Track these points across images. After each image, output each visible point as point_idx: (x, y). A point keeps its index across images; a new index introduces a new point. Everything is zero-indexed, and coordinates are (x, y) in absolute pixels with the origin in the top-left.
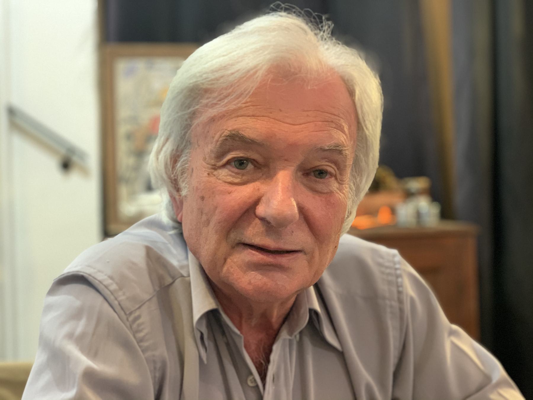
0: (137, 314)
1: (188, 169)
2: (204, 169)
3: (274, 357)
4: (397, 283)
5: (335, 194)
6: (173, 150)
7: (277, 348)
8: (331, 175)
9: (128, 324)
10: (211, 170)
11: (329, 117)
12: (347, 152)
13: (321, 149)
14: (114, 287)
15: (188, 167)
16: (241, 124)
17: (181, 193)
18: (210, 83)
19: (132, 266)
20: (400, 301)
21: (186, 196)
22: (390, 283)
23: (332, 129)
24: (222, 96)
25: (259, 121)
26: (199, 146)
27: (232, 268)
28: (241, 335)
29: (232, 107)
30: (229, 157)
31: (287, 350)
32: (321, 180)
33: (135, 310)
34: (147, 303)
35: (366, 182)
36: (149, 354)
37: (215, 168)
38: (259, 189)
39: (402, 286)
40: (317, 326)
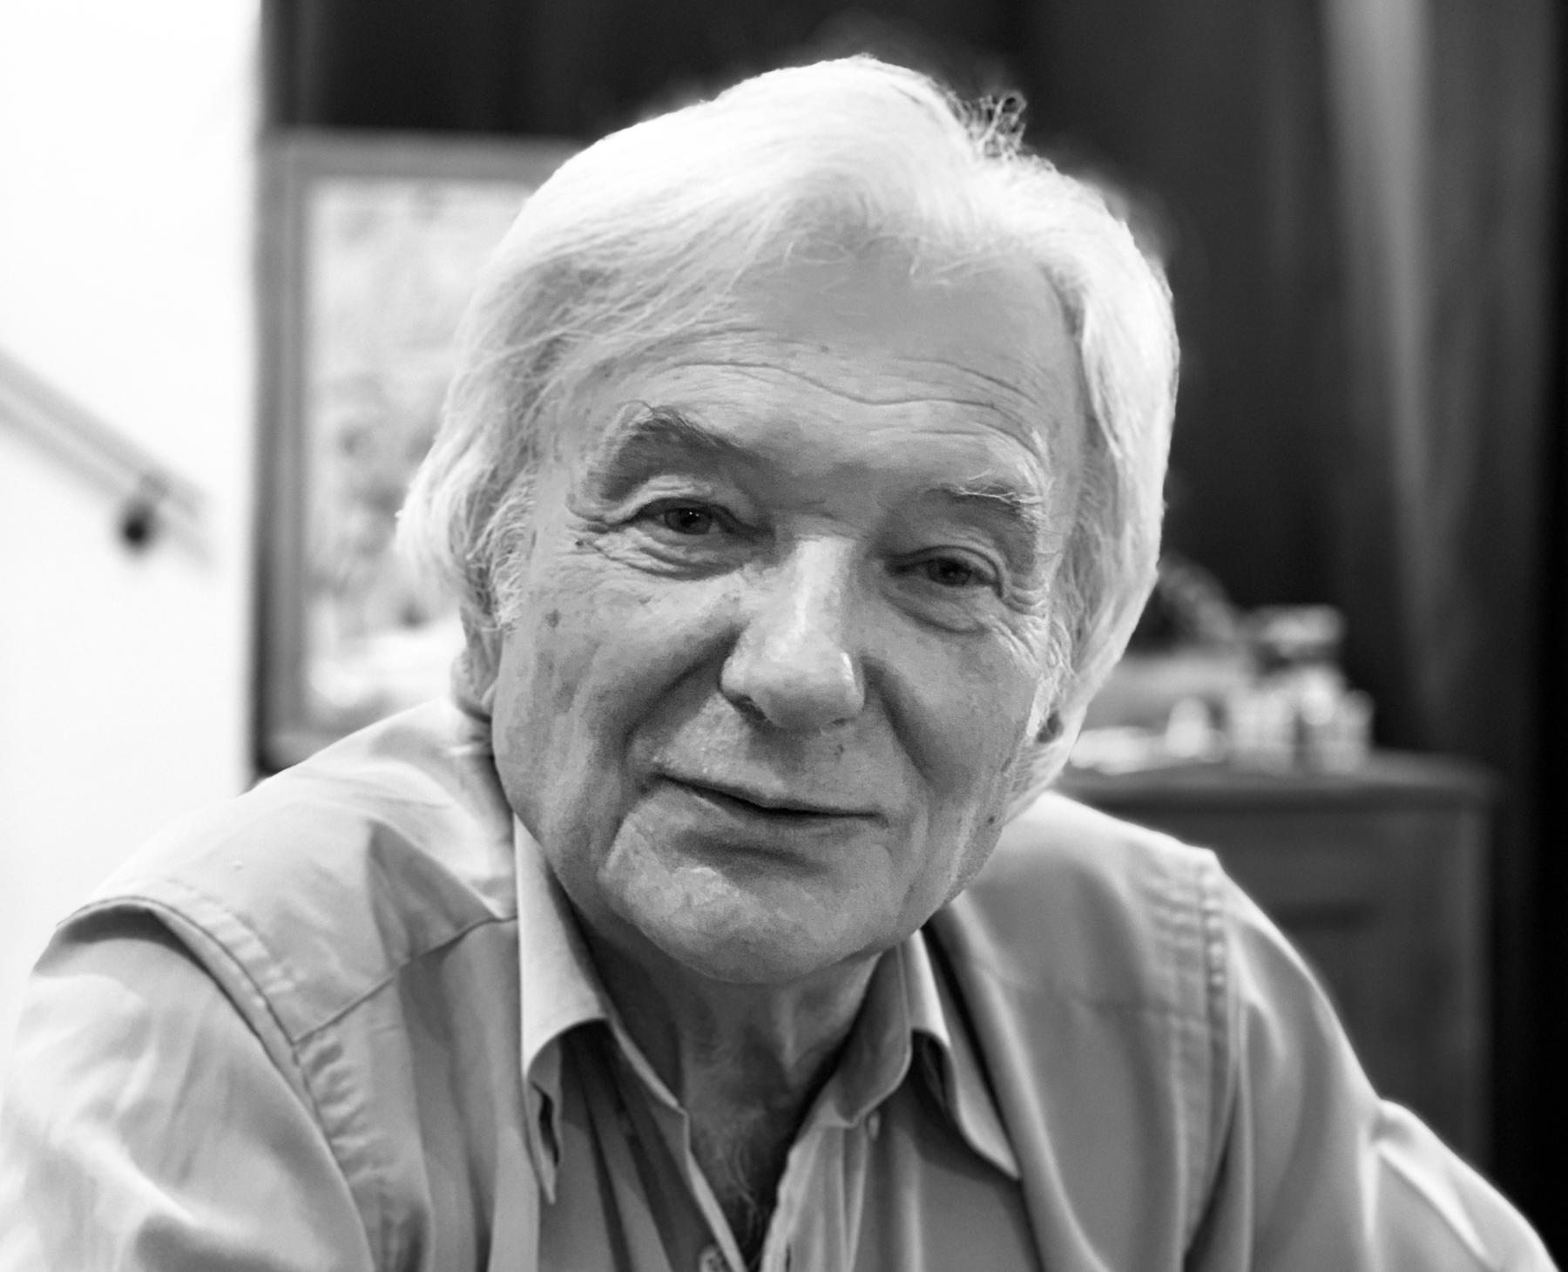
0: (329, 1040)
1: (521, 536)
2: (568, 531)
3: (792, 1188)
4: (1207, 959)
5: (996, 636)
6: (481, 476)
7: (802, 1160)
8: (981, 579)
9: (296, 1073)
10: (587, 533)
11: (983, 389)
12: (1037, 513)
13: (946, 491)
14: (252, 951)
15: (522, 528)
16: (696, 389)
17: (496, 615)
18: (604, 252)
19: (321, 883)
20: (1216, 1020)
21: (509, 626)
22: (1183, 959)
23: (990, 429)
24: (637, 296)
25: (751, 381)
26: (558, 458)
27: (637, 852)
28: (682, 1111)
29: (667, 329)
30: (646, 495)
31: (839, 1164)
32: (948, 590)
33: (323, 1029)
34: (365, 1006)
35: (1115, 620)
36: (365, 1174)
37: (601, 527)
38: (736, 600)
39: (1222, 970)
40: (935, 1088)
